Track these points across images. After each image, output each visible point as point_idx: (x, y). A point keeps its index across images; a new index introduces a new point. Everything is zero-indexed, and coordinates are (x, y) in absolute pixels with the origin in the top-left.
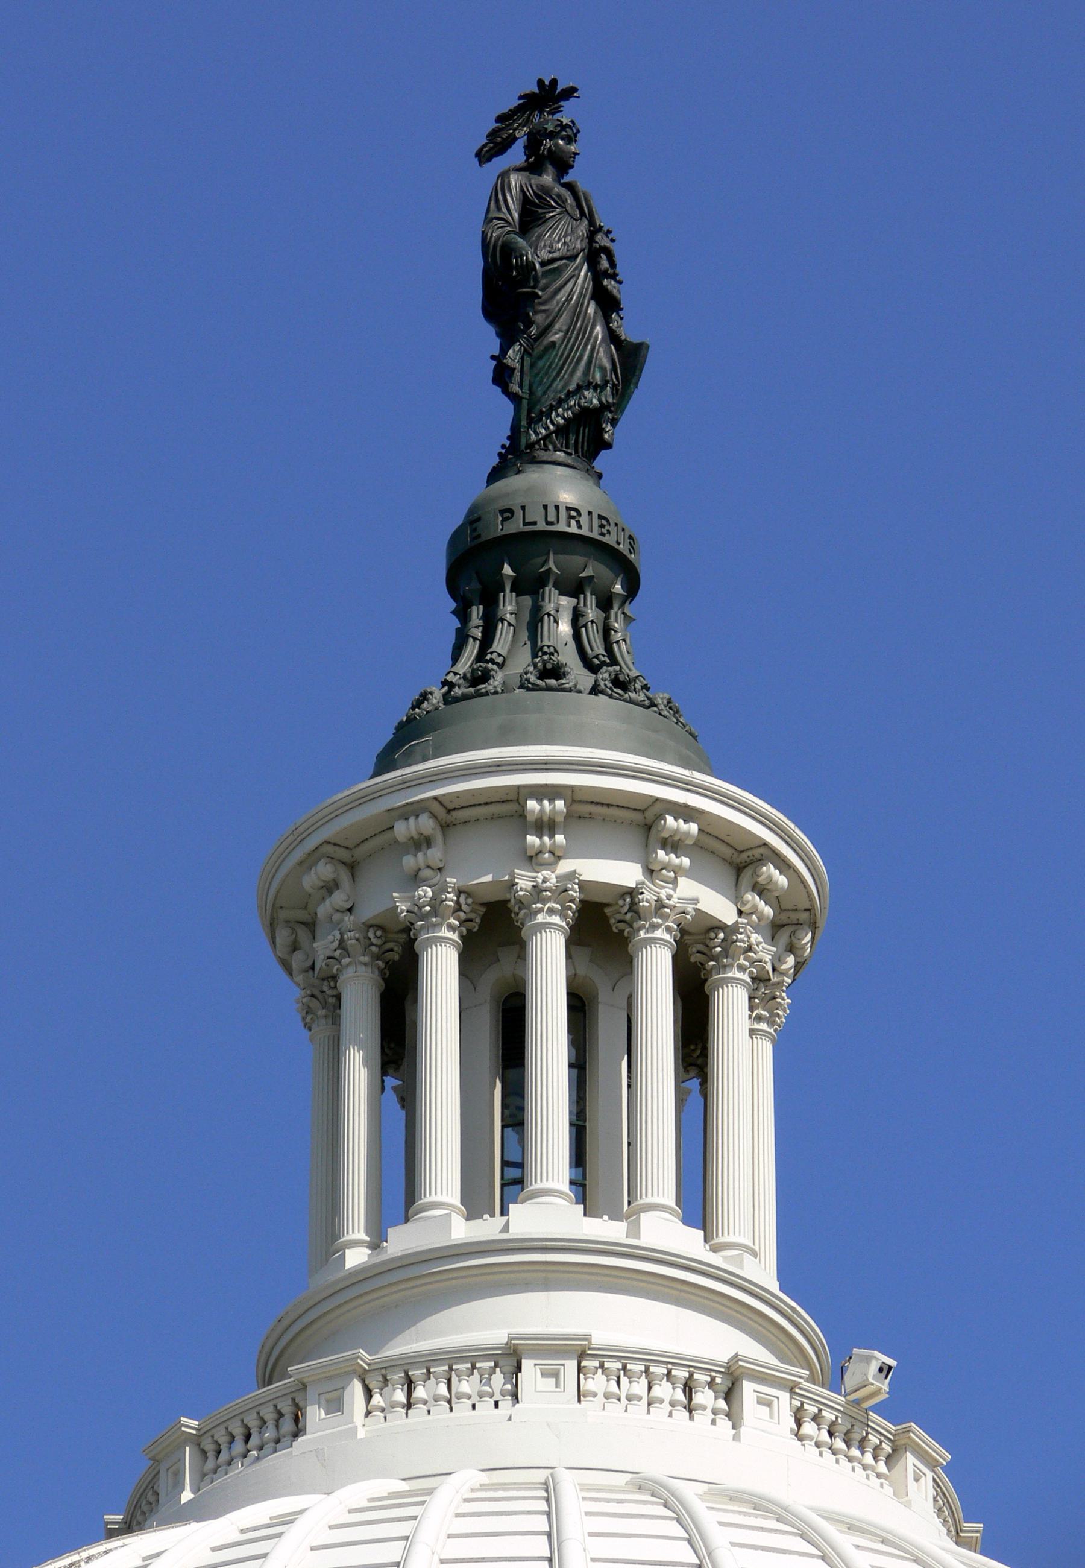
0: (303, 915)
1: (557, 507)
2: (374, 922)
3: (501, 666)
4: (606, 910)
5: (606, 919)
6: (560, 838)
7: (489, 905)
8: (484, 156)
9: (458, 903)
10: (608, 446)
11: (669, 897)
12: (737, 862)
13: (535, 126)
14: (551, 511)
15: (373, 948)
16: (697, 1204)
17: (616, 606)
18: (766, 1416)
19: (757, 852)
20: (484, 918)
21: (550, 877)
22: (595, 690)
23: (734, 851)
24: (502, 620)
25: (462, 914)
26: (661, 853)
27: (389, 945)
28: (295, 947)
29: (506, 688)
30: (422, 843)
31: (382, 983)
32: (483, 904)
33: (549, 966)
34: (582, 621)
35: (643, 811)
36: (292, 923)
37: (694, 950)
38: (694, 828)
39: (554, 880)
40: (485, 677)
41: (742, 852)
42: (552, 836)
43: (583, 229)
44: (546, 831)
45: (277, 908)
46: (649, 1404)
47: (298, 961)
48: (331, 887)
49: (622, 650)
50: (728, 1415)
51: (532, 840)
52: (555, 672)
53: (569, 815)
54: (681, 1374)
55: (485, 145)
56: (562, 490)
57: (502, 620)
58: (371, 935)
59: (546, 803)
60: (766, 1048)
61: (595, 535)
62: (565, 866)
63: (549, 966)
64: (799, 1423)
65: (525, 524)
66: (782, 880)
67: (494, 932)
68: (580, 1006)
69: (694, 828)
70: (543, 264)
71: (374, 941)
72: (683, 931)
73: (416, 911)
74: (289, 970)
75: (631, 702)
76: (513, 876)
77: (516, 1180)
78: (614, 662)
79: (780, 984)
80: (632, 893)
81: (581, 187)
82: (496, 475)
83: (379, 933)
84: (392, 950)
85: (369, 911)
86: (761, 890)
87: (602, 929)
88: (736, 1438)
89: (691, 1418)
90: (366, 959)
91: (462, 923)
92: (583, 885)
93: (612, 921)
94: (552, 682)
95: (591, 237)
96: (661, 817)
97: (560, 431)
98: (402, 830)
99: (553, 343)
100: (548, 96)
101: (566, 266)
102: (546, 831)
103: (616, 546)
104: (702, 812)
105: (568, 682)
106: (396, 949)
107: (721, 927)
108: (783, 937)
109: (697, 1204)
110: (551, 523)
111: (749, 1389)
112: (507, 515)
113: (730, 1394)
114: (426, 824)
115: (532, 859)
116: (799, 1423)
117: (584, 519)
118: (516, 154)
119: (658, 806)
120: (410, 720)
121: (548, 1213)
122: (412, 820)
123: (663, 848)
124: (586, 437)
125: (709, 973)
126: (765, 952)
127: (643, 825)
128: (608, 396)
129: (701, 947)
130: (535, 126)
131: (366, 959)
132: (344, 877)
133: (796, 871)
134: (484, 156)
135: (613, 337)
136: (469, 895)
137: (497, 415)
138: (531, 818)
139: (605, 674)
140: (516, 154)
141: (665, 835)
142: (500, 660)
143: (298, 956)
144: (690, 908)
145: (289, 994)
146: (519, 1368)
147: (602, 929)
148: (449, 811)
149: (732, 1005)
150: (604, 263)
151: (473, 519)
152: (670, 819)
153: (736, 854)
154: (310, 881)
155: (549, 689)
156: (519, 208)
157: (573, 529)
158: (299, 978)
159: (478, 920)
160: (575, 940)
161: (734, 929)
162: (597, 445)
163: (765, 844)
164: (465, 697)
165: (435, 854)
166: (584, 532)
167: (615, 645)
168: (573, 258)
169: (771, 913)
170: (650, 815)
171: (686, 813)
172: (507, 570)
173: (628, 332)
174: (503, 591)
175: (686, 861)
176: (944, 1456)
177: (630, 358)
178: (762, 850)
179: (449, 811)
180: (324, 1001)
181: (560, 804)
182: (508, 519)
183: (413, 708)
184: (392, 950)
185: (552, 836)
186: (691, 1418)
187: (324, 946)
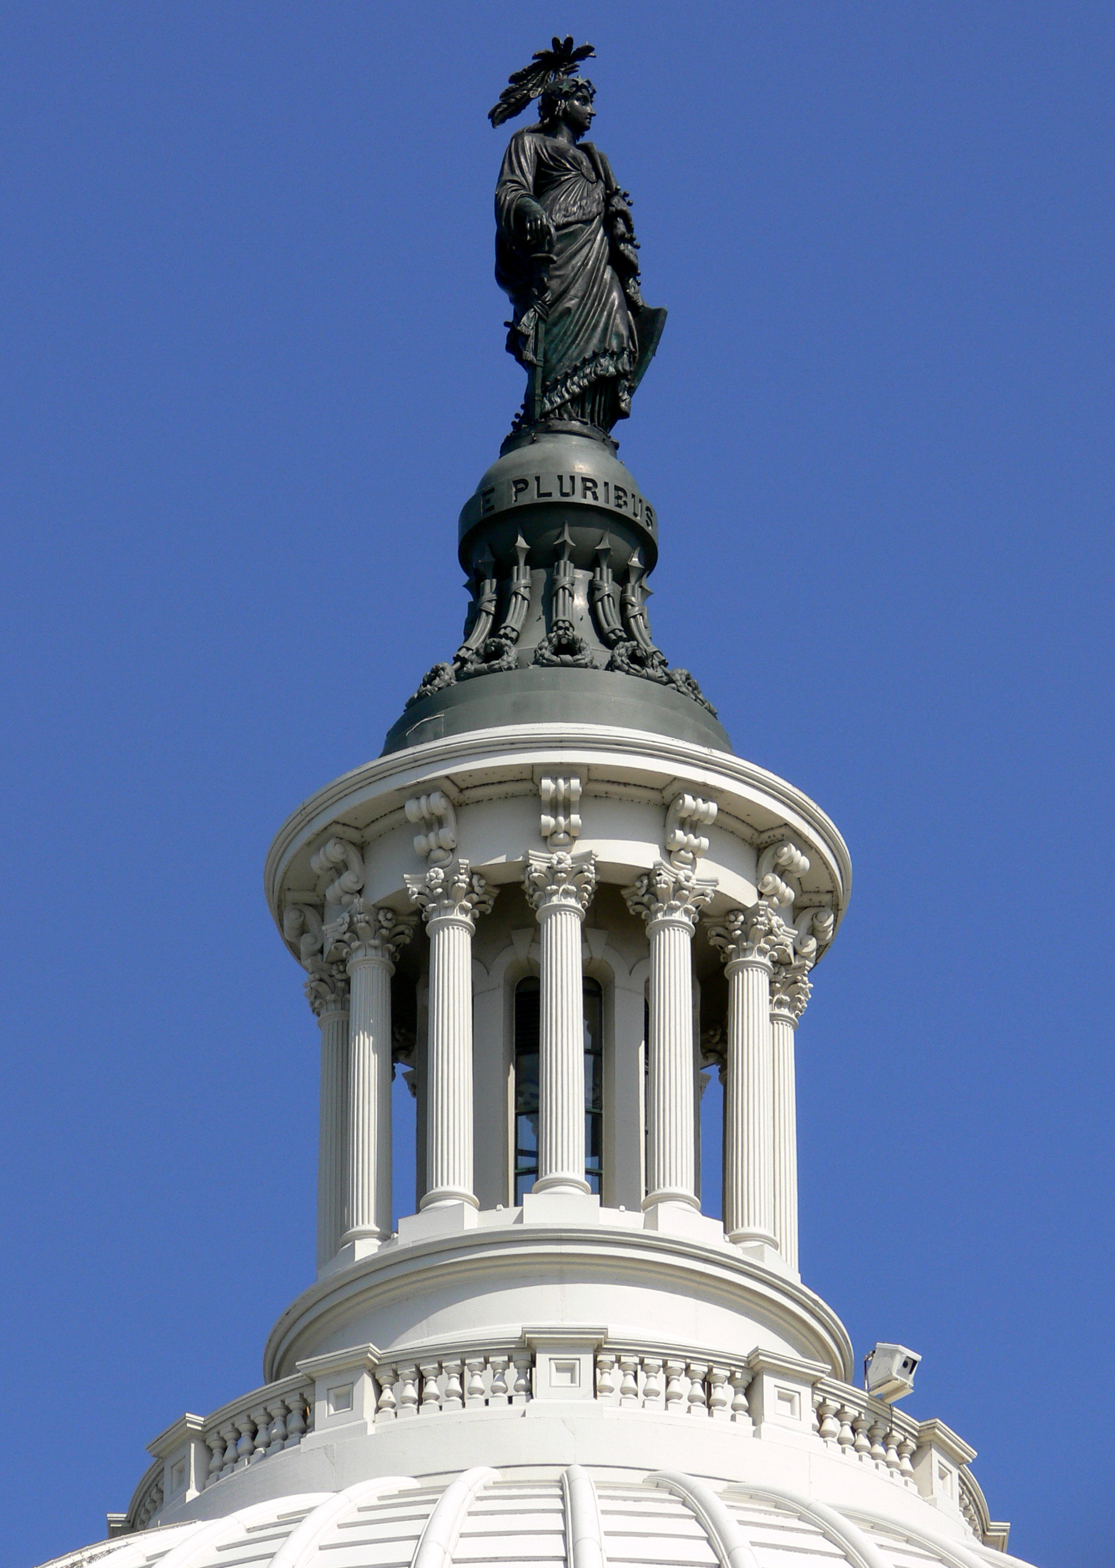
0: (310, 897)
1: (572, 478)
3: (515, 641)
4: (623, 892)
5: (623, 901)
6: (575, 818)
8: (497, 117)
9: (470, 884)
10: (625, 415)
11: (688, 879)
12: (757, 842)
15: (384, 931)
16: (717, 1193)
17: (633, 580)
18: (787, 1412)
19: (778, 833)
20: (497, 900)
21: (565, 858)
22: (611, 666)
23: (754, 832)
24: (516, 594)
25: (474, 896)
26: (679, 834)
27: (400, 928)
28: (303, 930)
29: (520, 664)
30: (434, 823)
31: (393, 967)
32: (496, 886)
34: (598, 595)
35: (661, 790)
36: (300, 905)
37: (714, 933)
38: (713, 807)
39: (569, 861)
40: (499, 652)
41: (762, 832)
42: (567, 816)
43: (599, 192)
44: (561, 810)
45: (284, 890)
46: (667, 1400)
47: (306, 944)
48: (339, 869)
49: (639, 625)
50: (748, 1411)
51: (547, 820)
52: (570, 647)
53: (585, 795)
54: (700, 1368)
55: (498, 106)
56: (577, 460)
57: (516, 594)
58: (381, 917)
59: (561, 782)
60: (787, 1034)
61: (611, 506)
62: (581, 847)
64: (821, 1419)
65: (540, 495)
67: (508, 915)
68: (596, 992)
69: (713, 807)
70: (558, 228)
71: (385, 923)
72: (702, 914)
73: (427, 893)
74: (297, 955)
75: (649, 678)
76: (527, 857)
78: (631, 637)
79: (801, 968)
80: (649, 874)
81: (597, 149)
82: (509, 444)
83: (389, 916)
84: (402, 933)
85: (379, 892)
86: (782, 872)
87: (619, 912)
88: (757, 1434)
89: (710, 1414)
90: (376, 942)
91: (475, 905)
92: (599, 866)
93: (629, 903)
94: (568, 658)
95: (607, 200)
96: (679, 796)
97: (576, 399)
98: (414, 810)
101: (582, 230)
102: (561, 810)
103: (633, 518)
104: (721, 791)
105: (584, 657)
106: (407, 932)
107: (743, 909)
108: (805, 920)
109: (717, 1193)
110: (567, 495)
111: (769, 1384)
112: (521, 486)
113: (750, 1389)
114: (438, 803)
115: (547, 840)
116: (821, 1419)
117: (600, 491)
118: (530, 116)
119: (676, 785)
120: (422, 696)
121: (564, 1203)
122: (423, 799)
123: (682, 828)
124: (603, 406)
125: (729, 957)
126: (787, 936)
127: (660, 805)
128: (625, 364)
129: (720, 930)
131: (376, 942)
132: (354, 858)
133: (818, 852)
134: (497, 117)
135: (630, 303)
136: (482, 876)
137: (514, 381)
138: (545, 797)
139: (621, 650)
140: (530, 116)
141: (684, 814)
142: (514, 635)
144: (709, 890)
145: (297, 978)
146: (533, 1363)
147: (619, 912)
148: (461, 790)
149: (752, 990)
150: (621, 227)
151: (486, 491)
152: (688, 799)
153: (756, 834)
154: (318, 862)
155: (564, 664)
156: (533, 170)
157: (589, 500)
158: (307, 962)
159: (491, 902)
160: (591, 923)
161: (755, 911)
162: (614, 414)
163: (786, 824)
164: (478, 673)
165: (447, 835)
167: (632, 620)
171: (705, 792)
172: (521, 542)
173: (646, 298)
174: (517, 564)
175: (705, 842)
176: (970, 1453)
177: (647, 324)
178: (783, 830)
179: (461, 790)
180: (333, 985)
181: (575, 783)
182: (522, 490)
183: (425, 685)
184: (402, 933)
185: (567, 816)
186: (710, 1414)
187: (333, 928)
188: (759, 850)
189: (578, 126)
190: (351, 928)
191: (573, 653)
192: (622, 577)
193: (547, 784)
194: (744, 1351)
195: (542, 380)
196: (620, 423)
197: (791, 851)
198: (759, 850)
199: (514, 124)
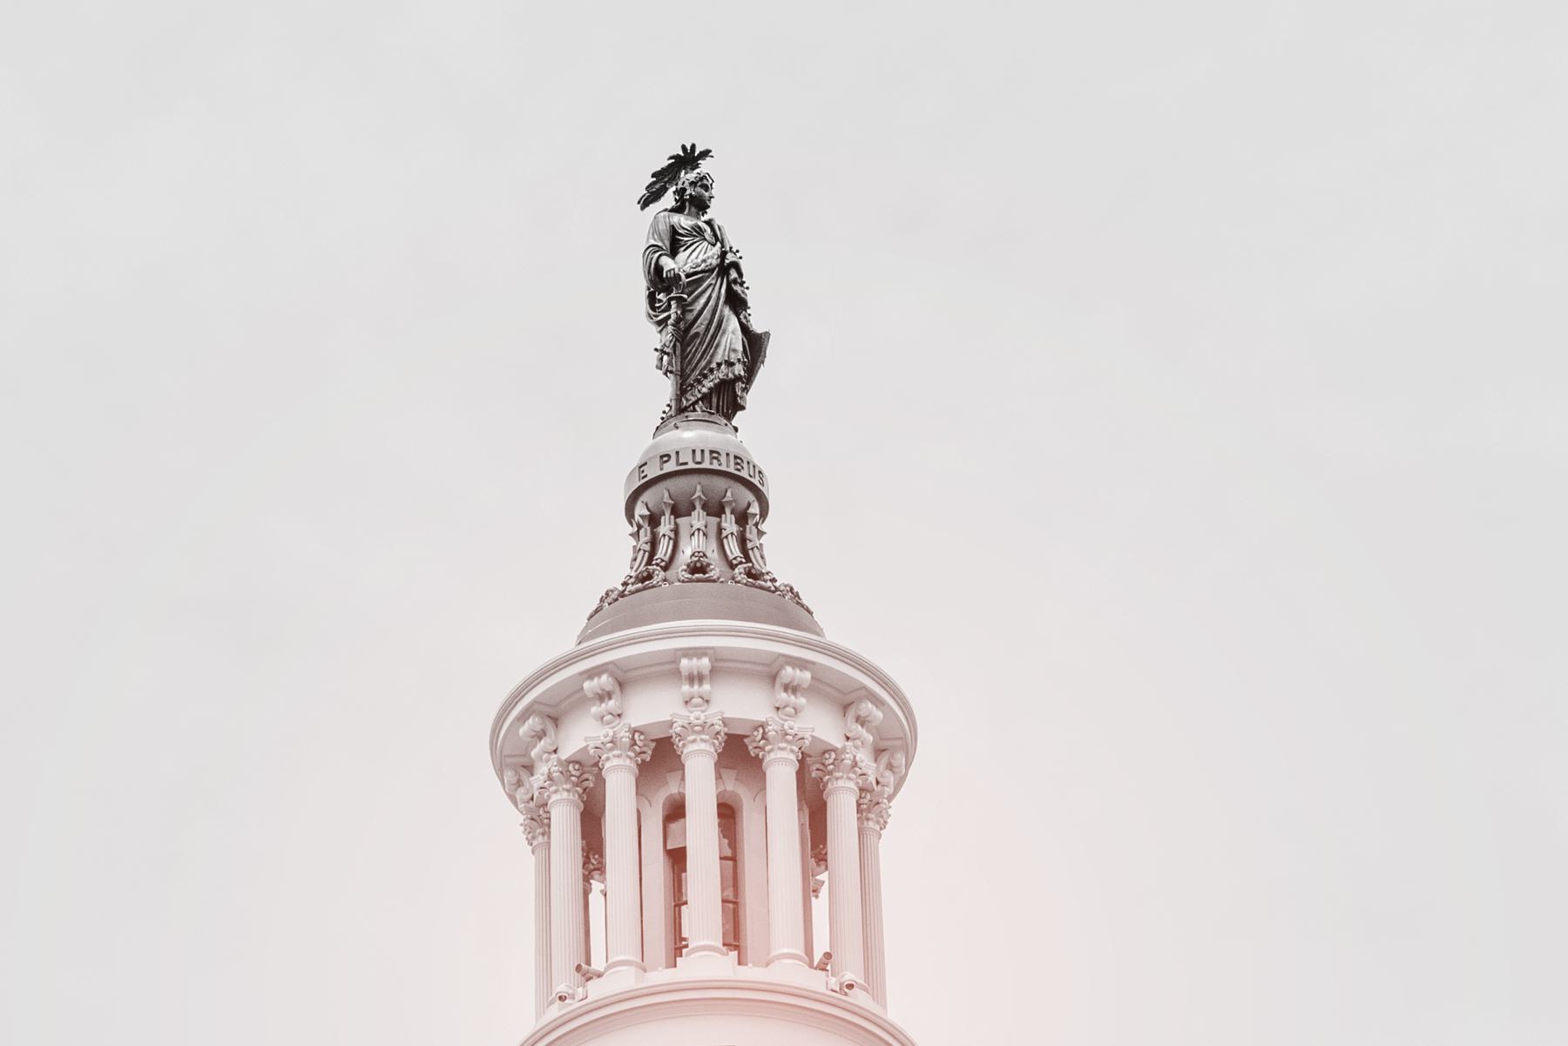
2: (577, 758)
6: (706, 687)
7: (657, 741)
8: (645, 203)
10: (743, 408)
13: (681, 180)
14: (698, 454)
17: (751, 522)
28: (519, 784)
33: (700, 781)
34: (725, 533)
36: (514, 765)
38: (807, 675)
40: (650, 577)
43: (717, 249)
47: (521, 794)
48: (541, 735)
61: (732, 470)
63: (700, 781)
65: (678, 464)
66: (879, 714)
67: (660, 757)
68: (728, 814)
69: (807, 675)
70: (688, 276)
74: (515, 803)
75: (761, 588)
77: (678, 946)
78: (748, 559)
81: (717, 223)
86: (861, 720)
89: (705, 154)
90: (568, 786)
92: (725, 722)
95: (723, 255)
97: (706, 398)
99: (697, 334)
100: (689, 158)
104: (813, 663)
105: (713, 574)
107: (834, 750)
108: (884, 759)
117: (723, 459)
118: (669, 200)
119: (863, 692)
124: (726, 400)
125: (826, 784)
128: (739, 369)
130: (681, 180)
131: (568, 786)
134: (645, 203)
135: (745, 329)
137: (665, 388)
138: (685, 673)
139: (740, 569)
140: (669, 200)
143: (521, 790)
144: (807, 735)
145: (515, 819)
147: (739, 753)
150: (734, 274)
152: (789, 670)
155: (698, 581)
157: (715, 466)
158: (521, 806)
161: (844, 749)
162: (734, 406)
163: (865, 688)
166: (723, 468)
168: (712, 271)
169: (871, 738)
170: (849, 699)
171: (802, 664)
173: (757, 326)
177: (755, 345)
180: (538, 821)
186: (705, 154)
187: (538, 779)
188: (845, 708)
189: (700, 205)
190: (550, 778)
191: (705, 573)
192: (742, 518)
193: (684, 662)
194: (498, 862)
195: (682, 391)
196: (739, 413)
197: (868, 708)
198: (845, 708)
199: (655, 208)
